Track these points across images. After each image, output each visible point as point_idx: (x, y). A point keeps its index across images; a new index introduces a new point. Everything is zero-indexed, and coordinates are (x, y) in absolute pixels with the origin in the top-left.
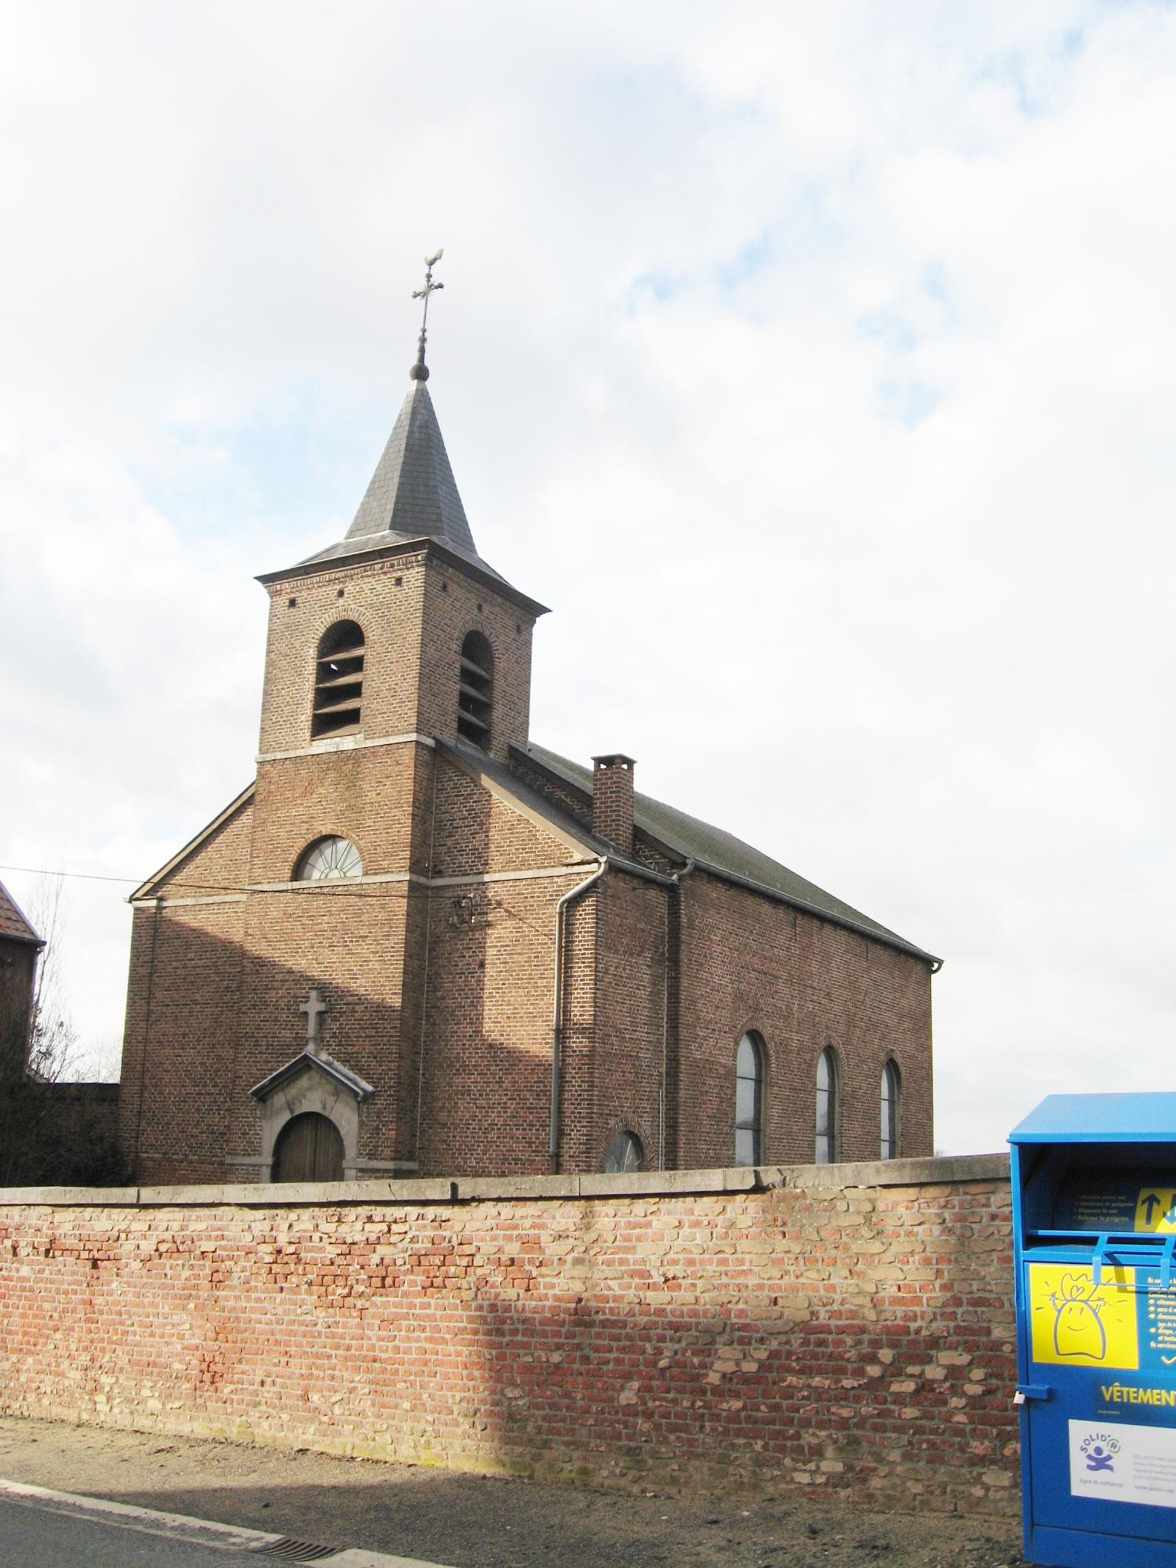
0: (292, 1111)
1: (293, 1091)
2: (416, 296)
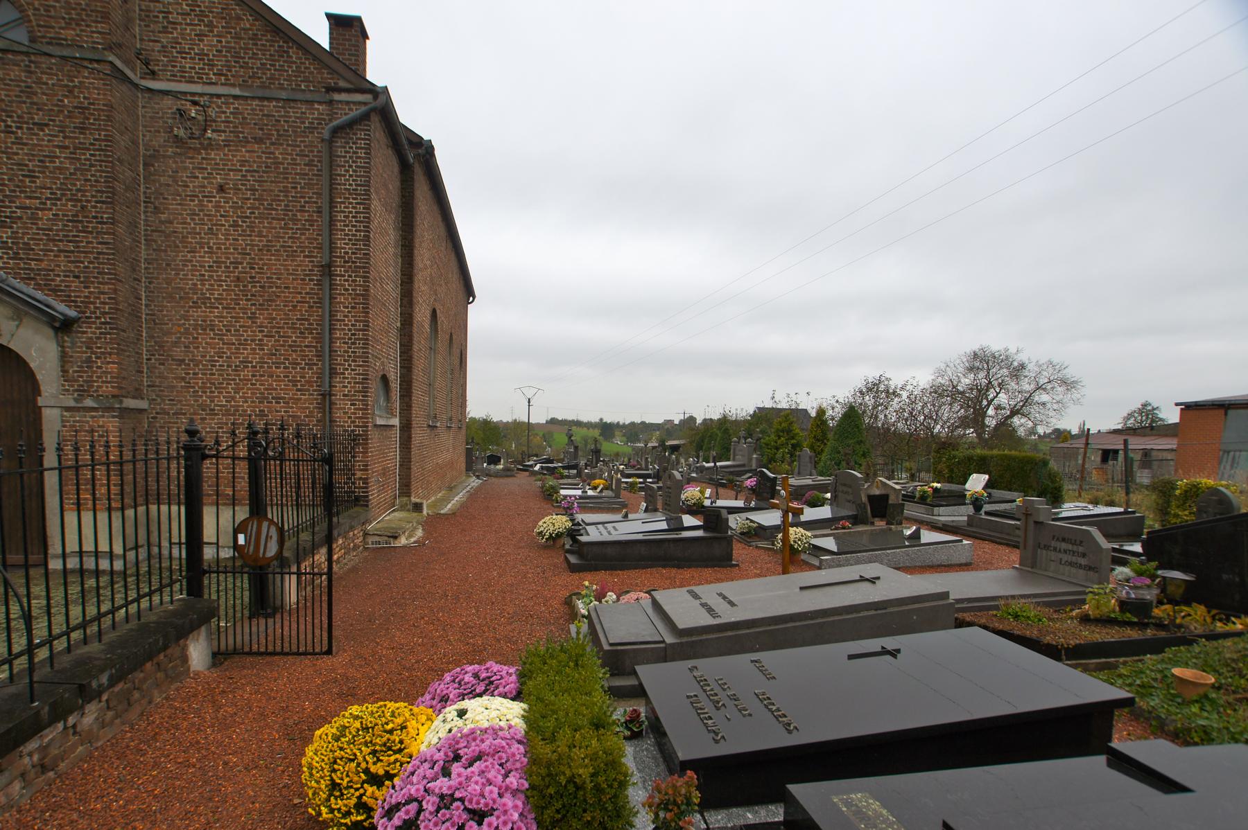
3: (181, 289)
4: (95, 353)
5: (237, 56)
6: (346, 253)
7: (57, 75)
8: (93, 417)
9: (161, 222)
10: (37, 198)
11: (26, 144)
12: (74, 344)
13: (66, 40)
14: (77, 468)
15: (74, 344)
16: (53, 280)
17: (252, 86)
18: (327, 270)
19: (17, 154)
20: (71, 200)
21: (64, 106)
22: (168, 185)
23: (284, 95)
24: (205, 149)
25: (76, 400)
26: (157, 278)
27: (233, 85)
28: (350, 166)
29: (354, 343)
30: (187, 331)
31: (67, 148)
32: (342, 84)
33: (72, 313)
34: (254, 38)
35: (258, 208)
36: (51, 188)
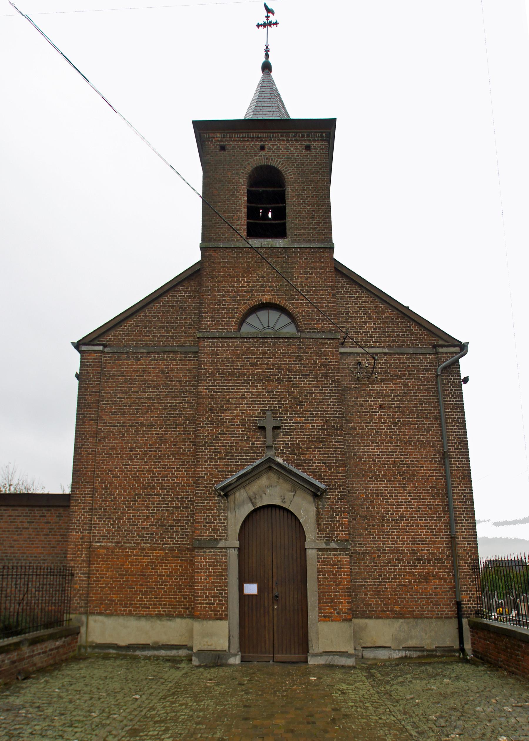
0: (253, 504)
1: (254, 487)
2: (258, 26)
3: (363, 470)
4: (335, 512)
5: (384, 332)
6: (455, 443)
7: (313, 348)
8: (334, 555)
9: (350, 429)
10: (303, 417)
11: (298, 387)
12: (323, 506)
13: (317, 329)
14: (512, 566)
15: (323, 506)
16: (312, 466)
17: (393, 347)
18: (445, 455)
19: (294, 392)
20: (320, 417)
21: (317, 364)
22: (353, 406)
23: (411, 351)
24: (371, 384)
25: (326, 544)
26: (349, 464)
27: (383, 347)
28: (452, 390)
29: (465, 502)
30: (367, 498)
31: (318, 387)
32: (441, 342)
33: (322, 486)
34: (392, 321)
35: (402, 418)
36: (310, 411)
